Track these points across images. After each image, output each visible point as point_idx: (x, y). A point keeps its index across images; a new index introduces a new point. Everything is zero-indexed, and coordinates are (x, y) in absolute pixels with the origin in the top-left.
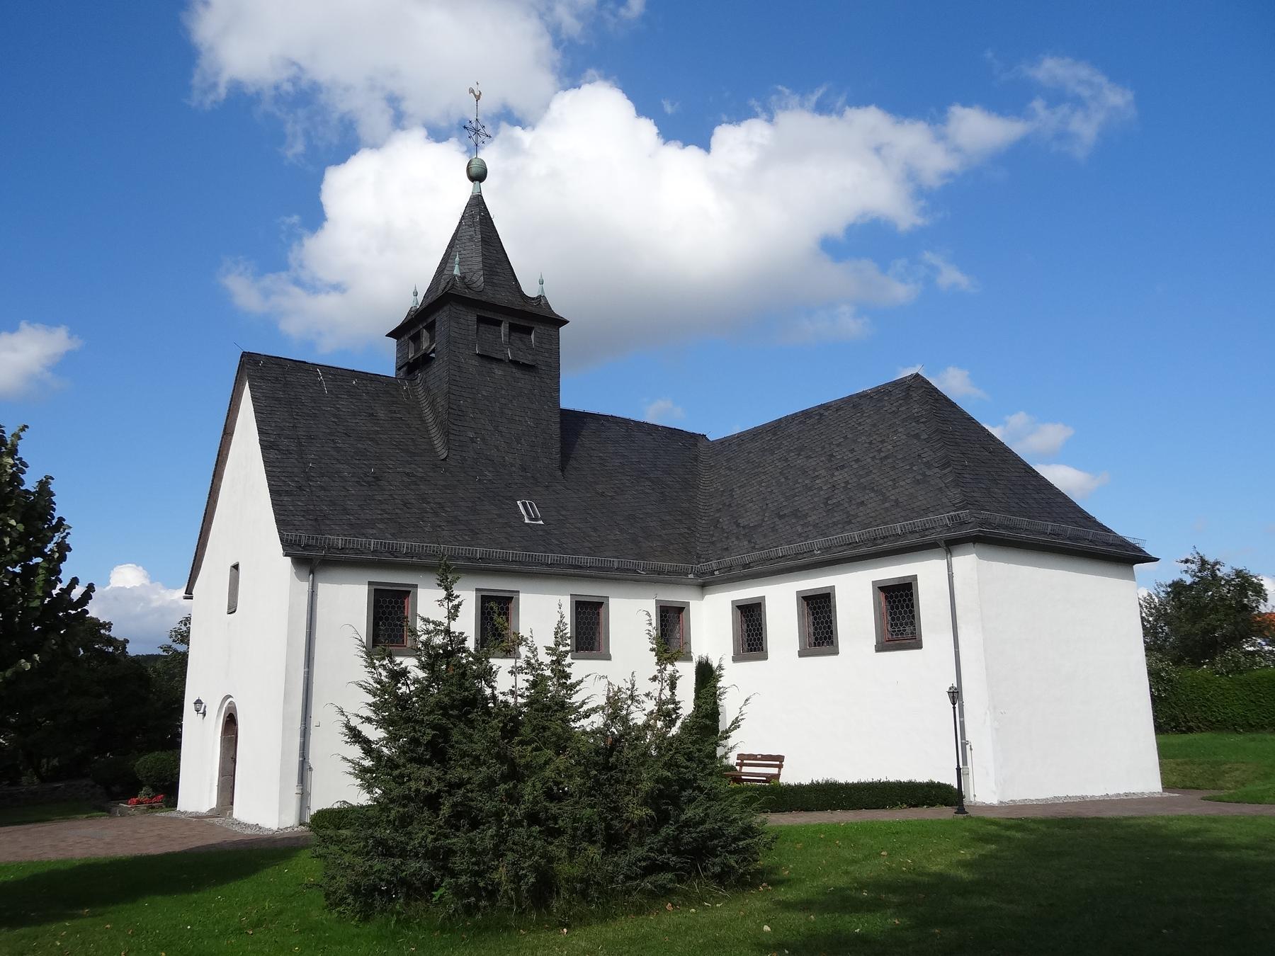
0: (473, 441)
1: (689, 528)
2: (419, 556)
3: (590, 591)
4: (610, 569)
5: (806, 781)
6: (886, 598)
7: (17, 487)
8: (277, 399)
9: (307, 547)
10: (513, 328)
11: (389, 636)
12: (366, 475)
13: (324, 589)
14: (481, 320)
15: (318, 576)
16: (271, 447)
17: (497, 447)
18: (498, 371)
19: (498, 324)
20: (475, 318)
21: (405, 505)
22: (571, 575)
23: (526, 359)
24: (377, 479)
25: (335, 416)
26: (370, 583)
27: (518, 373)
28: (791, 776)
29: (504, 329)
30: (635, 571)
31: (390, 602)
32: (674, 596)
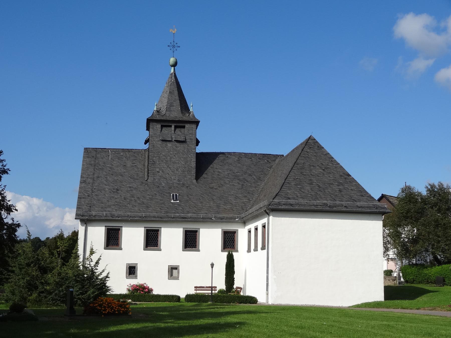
0: (158, 172)
1: (249, 199)
2: (122, 217)
3: (191, 227)
4: (200, 218)
5: (118, 293)
6: (189, 247)
7: (4, 209)
8: (91, 164)
9: (82, 216)
10: (176, 127)
11: (116, 240)
12: (114, 189)
13: (90, 229)
14: (162, 126)
15: (88, 225)
16: (83, 182)
17: (168, 174)
18: (169, 145)
19: (171, 126)
20: (160, 126)
21: (125, 199)
22: (183, 221)
23: (182, 139)
24: (118, 190)
25: (111, 168)
26: (105, 226)
27: (178, 144)
28: (155, 292)
29: (173, 127)
30: (211, 219)
31: (114, 232)
32: (230, 227)
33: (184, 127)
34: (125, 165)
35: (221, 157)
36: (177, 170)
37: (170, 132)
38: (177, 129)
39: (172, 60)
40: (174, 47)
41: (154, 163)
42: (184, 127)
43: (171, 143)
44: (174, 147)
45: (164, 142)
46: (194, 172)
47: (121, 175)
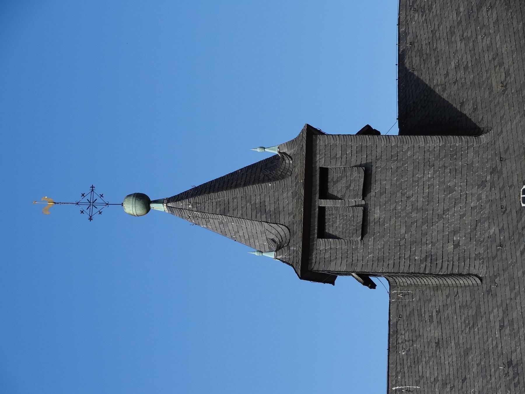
0: (457, 245)
10: (325, 195)
14: (323, 234)
18: (376, 214)
19: (322, 210)
24: (510, 363)
27: (375, 188)
29: (323, 203)
33: (324, 172)
34: (438, 344)
35: (410, 63)
36: (451, 190)
37: (340, 212)
38: (330, 191)
39: (131, 208)
40: (92, 204)
41: (429, 257)
42: (324, 172)
43: (371, 208)
44: (383, 199)
45: (371, 227)
46: (456, 142)
47: (467, 353)
